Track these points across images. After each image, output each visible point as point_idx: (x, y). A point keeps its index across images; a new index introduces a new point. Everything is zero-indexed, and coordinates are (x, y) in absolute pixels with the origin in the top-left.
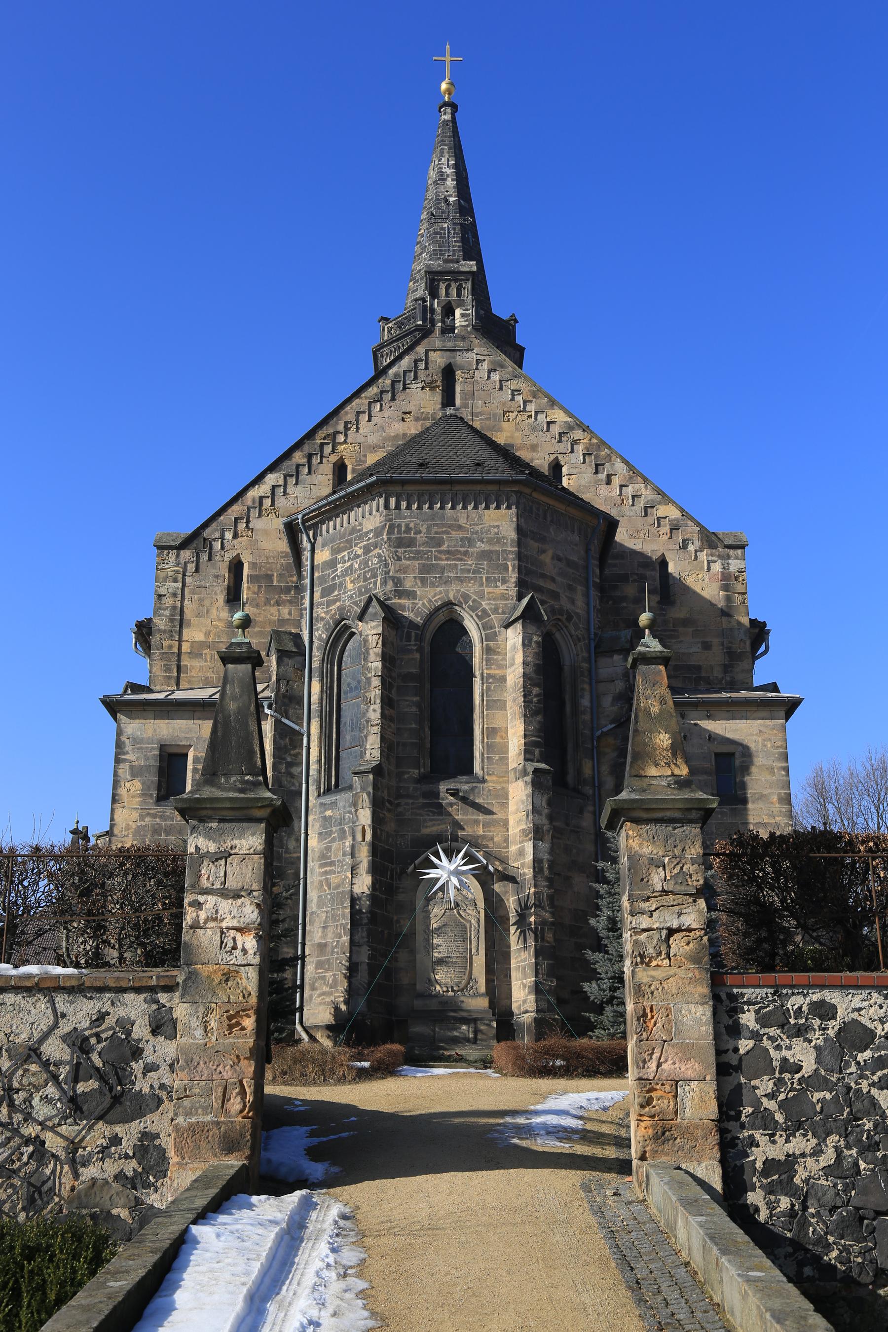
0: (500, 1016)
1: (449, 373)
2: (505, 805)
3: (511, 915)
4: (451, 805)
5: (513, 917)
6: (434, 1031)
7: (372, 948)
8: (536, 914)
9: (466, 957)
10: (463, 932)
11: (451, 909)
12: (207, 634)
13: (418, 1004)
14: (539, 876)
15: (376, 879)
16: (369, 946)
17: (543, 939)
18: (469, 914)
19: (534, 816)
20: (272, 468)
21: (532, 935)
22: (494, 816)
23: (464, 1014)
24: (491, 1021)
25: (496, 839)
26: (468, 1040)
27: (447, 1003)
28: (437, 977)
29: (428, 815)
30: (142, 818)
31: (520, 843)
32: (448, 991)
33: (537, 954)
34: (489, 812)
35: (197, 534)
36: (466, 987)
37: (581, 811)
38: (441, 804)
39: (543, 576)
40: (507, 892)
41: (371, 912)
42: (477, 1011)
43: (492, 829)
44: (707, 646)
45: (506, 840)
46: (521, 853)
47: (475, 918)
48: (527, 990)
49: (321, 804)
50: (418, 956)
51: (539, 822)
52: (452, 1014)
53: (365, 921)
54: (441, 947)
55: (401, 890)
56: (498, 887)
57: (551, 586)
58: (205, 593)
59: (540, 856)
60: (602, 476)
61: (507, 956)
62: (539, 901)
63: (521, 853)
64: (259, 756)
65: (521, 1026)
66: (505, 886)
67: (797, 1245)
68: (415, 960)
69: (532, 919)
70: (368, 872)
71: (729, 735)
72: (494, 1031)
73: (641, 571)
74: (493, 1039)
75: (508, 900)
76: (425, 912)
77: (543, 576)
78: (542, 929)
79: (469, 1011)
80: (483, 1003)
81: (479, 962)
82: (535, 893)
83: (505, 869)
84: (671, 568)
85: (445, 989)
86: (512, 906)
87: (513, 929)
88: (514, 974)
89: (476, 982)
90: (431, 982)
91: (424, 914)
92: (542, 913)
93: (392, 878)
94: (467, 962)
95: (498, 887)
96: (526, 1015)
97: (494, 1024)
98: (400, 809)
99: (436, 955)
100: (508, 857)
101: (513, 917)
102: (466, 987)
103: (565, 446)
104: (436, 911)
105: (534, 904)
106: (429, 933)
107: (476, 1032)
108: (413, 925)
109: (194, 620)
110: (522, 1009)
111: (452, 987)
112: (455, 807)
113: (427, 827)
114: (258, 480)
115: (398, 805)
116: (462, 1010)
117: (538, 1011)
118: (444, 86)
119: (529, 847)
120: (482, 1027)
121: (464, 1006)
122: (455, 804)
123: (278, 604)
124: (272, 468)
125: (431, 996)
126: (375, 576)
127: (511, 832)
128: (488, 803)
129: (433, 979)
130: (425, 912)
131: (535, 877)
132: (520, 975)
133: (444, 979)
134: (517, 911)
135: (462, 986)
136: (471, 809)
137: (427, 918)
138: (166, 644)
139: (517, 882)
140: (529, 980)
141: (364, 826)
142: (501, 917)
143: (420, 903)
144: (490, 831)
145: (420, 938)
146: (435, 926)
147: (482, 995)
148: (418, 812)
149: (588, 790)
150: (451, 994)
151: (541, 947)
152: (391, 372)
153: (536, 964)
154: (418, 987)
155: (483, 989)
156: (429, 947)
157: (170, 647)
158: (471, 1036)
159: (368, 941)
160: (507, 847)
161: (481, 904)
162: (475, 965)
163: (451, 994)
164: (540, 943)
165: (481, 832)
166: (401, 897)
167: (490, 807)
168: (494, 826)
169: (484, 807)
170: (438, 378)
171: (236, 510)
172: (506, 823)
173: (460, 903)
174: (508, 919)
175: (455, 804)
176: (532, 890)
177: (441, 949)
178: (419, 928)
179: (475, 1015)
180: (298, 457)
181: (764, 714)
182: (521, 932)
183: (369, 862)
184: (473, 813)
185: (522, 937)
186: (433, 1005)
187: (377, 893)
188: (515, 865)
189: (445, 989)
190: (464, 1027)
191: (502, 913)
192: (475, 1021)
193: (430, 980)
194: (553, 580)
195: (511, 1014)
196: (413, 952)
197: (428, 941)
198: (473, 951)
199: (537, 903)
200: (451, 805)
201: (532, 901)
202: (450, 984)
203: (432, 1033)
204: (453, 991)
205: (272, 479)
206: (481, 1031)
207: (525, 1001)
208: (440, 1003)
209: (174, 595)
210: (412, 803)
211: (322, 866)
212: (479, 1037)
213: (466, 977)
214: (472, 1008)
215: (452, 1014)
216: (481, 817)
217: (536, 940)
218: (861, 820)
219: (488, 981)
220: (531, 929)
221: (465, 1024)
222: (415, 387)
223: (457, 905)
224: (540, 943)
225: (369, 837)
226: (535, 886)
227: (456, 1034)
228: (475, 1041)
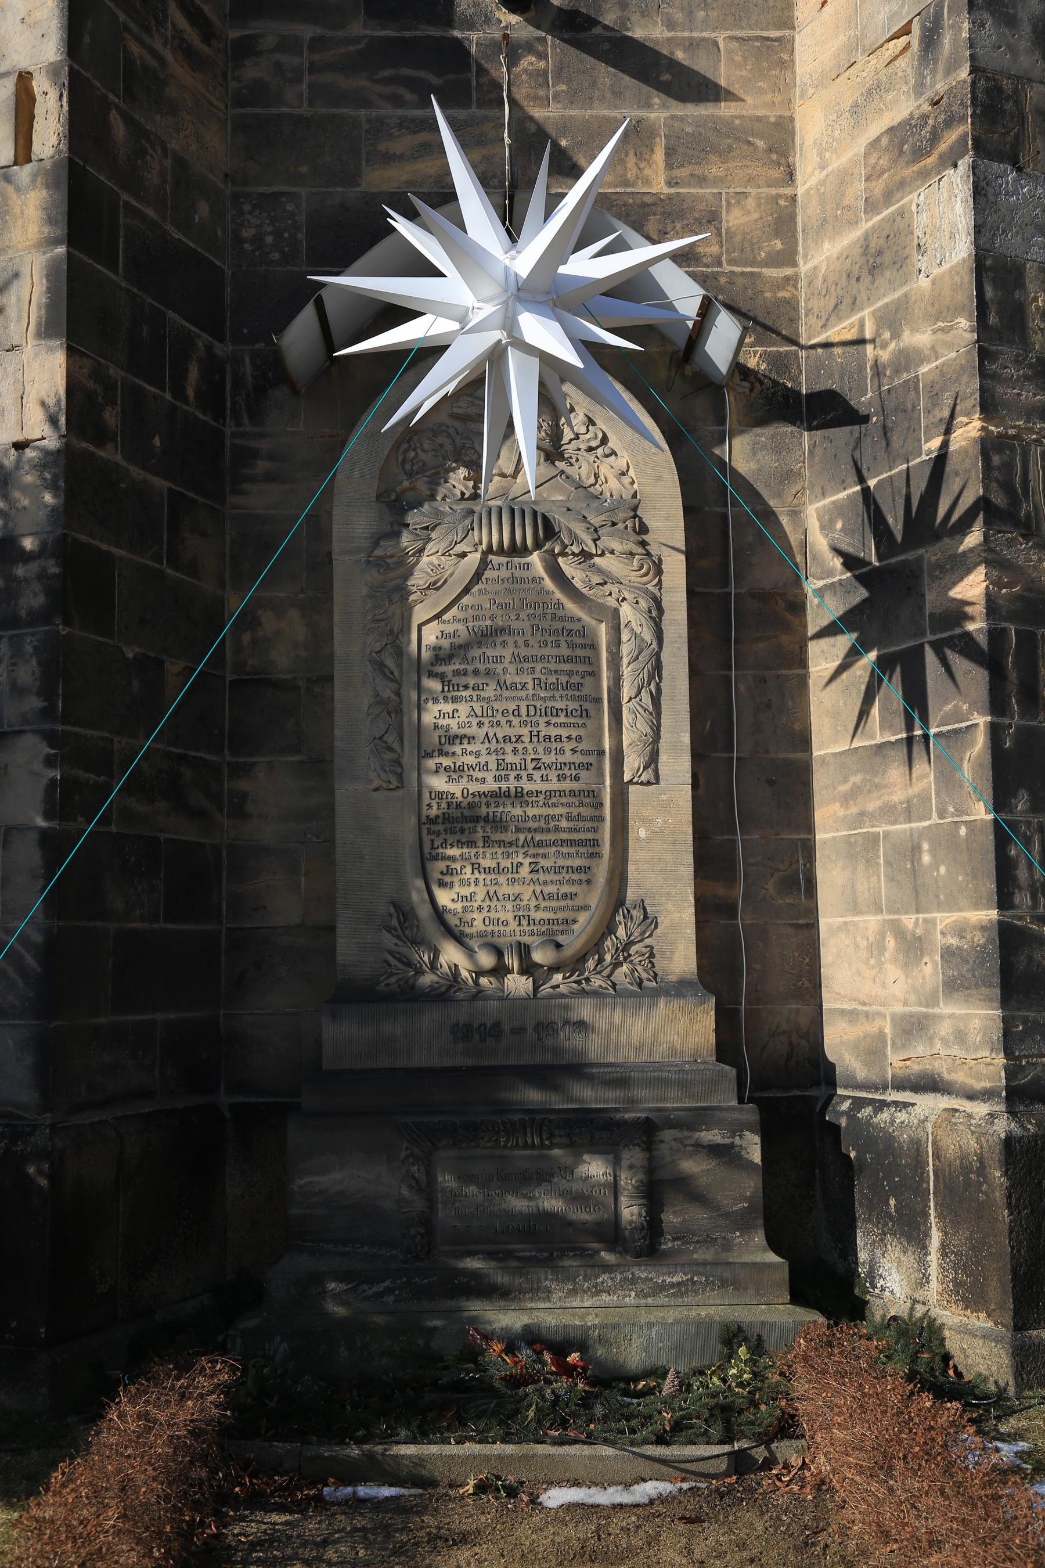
0: (761, 1083)
2: (775, 53)
3: (811, 586)
4: (513, 50)
5: (825, 591)
6: (427, 1189)
7: (65, 750)
9: (593, 796)
10: (574, 663)
11: (517, 550)
13: (344, 1037)
14: (1007, 352)
15: (98, 374)
16: (51, 738)
18: (607, 578)
19: (977, 25)
21: (974, 678)
22: (725, 110)
23: (594, 1097)
24: (736, 1129)
25: (734, 219)
26: (611, 1234)
27: (494, 1030)
28: (444, 898)
29: (397, 101)
31: (871, 206)
32: (500, 971)
33: (1006, 775)
34: (698, 88)
36: (596, 946)
38: (460, 48)
40: (788, 476)
41: (62, 548)
42: (659, 1075)
43: (715, 170)
45: (783, 221)
46: (883, 256)
47: (640, 599)
48: (930, 970)
50: (345, 792)
51: (999, 60)
52: (533, 1096)
53: (33, 599)
54: (473, 739)
55: (262, 466)
56: (745, 453)
59: (1009, 244)
61: (790, 787)
62: (1007, 487)
63: (883, 256)
66: (778, 448)
67: (905, 1107)
68: (330, 809)
69: (973, 587)
70: (46, 331)
72: (751, 1186)
74: (742, 1222)
75: (795, 514)
76: (381, 564)
78: (1027, 641)
79: (618, 1078)
80: (686, 1030)
81: (662, 821)
82: (987, 446)
83: (780, 362)
85: (487, 960)
86: (820, 542)
87: (823, 657)
88: (831, 879)
89: (650, 922)
90: (414, 925)
91: (373, 576)
92: (1022, 552)
93: (212, 397)
94: (598, 829)
95: (745, 453)
96: (928, 1106)
97: (753, 1149)
98: (252, 71)
99: (438, 783)
100: (791, 304)
101: (825, 591)
102: (596, 946)
104: (442, 567)
105: (983, 505)
106: (401, 674)
107: (654, 1192)
108: (321, 638)
110: (895, 1062)
111: (523, 951)
112: (528, 61)
113: (389, 159)
115: (245, 49)
116: (577, 1070)
117: (1018, 1095)
120: (691, 1166)
121: (588, 1047)
122: (529, 47)
125: (410, 996)
128: (692, 45)
129: (424, 912)
130: (381, 564)
131: (984, 354)
132: (876, 882)
133: (485, 907)
134: (850, 562)
135: (573, 942)
136: (606, 74)
137: (393, 591)
139: (853, 417)
140: (944, 919)
141: (24, 79)
142: (765, 597)
144: (702, 180)
145: (352, 699)
146: (431, 636)
147: (678, 989)
148: (346, 83)
150: (518, 984)
151: (1025, 736)
153: (1001, 838)
154: (348, 948)
155: (681, 957)
156: (404, 747)
158: (630, 1211)
159: (47, 713)
160: (788, 257)
161: (668, 525)
162: (638, 832)
163: (518, 984)
164: (1015, 720)
165: (659, 186)
166: (259, 499)
167: (701, 64)
168: (724, 154)
169: (673, 65)
172: (779, 142)
173: (560, 519)
174: (798, 607)
175: (529, 47)
176: (969, 429)
177: (464, 756)
178: (350, 647)
179: (651, 1101)
182: (884, 664)
183: (52, 273)
184: (618, 94)
185: (893, 691)
186: (426, 1042)
187: (111, 454)
188: (840, 331)
189: (487, 960)
190: (595, 1169)
191: (764, 577)
192: (646, 1131)
193: (404, 914)
195: (822, 1073)
196: (320, 768)
198: (632, 763)
199: (999, 499)
200: (513, 50)
201: (965, 487)
202: (513, 931)
203: (419, 1204)
204: (528, 968)
208: (463, 1032)
210: (317, 43)
212: (670, 1218)
213: (595, 897)
214: (628, 1056)
215: (533, 1096)
216: (661, 112)
217: (997, 705)
219: (708, 910)
220: (967, 646)
221: (596, 1147)
223: (548, 530)
224: (1015, 720)
225: (49, 134)
226: (988, 407)
227: (551, 1203)
228: (648, 1244)
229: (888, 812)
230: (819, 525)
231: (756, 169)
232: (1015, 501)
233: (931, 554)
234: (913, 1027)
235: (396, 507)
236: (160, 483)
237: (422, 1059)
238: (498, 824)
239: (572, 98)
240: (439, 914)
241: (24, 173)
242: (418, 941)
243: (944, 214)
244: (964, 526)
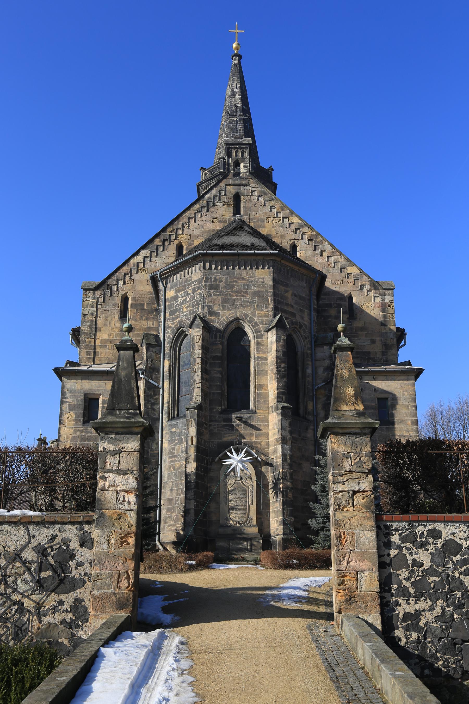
0: (264, 537)
1: (237, 197)
2: (267, 426)
3: (270, 484)
4: (238, 425)
5: (271, 485)
6: (229, 545)
7: (196, 501)
8: (283, 483)
9: (246, 506)
10: (244, 492)
11: (238, 480)
12: (109, 335)
13: (221, 530)
14: (285, 463)
15: (199, 465)
16: (195, 500)
18: (248, 483)
19: (282, 431)
20: (144, 247)
21: (281, 494)
22: (261, 432)
23: (245, 536)
24: (260, 540)
25: (262, 444)
26: (247, 550)
27: (236, 530)
28: (231, 516)
29: (226, 431)
30: (75, 432)
31: (275, 445)
32: (236, 524)
33: (284, 504)
34: (258, 429)
35: (104, 282)
36: (246, 521)
37: (307, 429)
38: (233, 425)
39: (287, 304)
40: (268, 471)
41: (196, 482)
42: (252, 534)
43: (260, 438)
44: (373, 342)
45: (267, 444)
46: (275, 451)
47: (251, 485)
48: (278, 523)
49: (170, 425)
50: (221, 505)
52: (239, 536)
53: (193, 487)
54: (233, 500)
55: (212, 470)
56: (263, 469)
57: (291, 310)
58: (108, 313)
59: (285, 452)
60: (318, 252)
61: (268, 505)
62: (285, 476)
63: (275, 451)
64: (137, 399)
66: (267, 468)
67: (421, 658)
68: (219, 507)
69: (281, 486)
70: (194, 461)
71: (385, 389)
72: (261, 545)
73: (339, 302)
75: (268, 476)
76: (225, 482)
77: (287, 304)
78: (286, 491)
79: (247, 534)
80: (255, 530)
81: (253, 508)
82: (283, 472)
83: (267, 459)
84: (354, 300)
85: (235, 523)
86: (271, 479)
87: (271, 491)
88: (271, 515)
89: (252, 519)
90: (228, 519)
92: (286, 482)
93: (207, 464)
94: (247, 509)
95: (263, 469)
96: (278, 537)
97: (261, 541)
98: (211, 428)
99: (230, 505)
100: (268, 453)
101: (271, 485)
102: (246, 521)
103: (298, 236)
104: (230, 481)
106: (226, 493)
107: (251, 545)
108: (218, 489)
109: (103, 328)
111: (239, 522)
113: (225, 437)
114: (136, 253)
115: (210, 425)
116: (244, 534)
117: (284, 534)
118: (234, 45)
120: (255, 543)
121: (245, 531)
122: (240, 425)
123: (147, 319)
124: (144, 247)
125: (227, 526)
126: (198, 304)
128: (258, 425)
129: (229, 518)
130: (225, 482)
131: (282, 463)
132: (274, 515)
133: (235, 517)
134: (273, 482)
135: (244, 521)
136: (248, 428)
137: (226, 485)
138: (87, 340)
140: (279, 518)
141: (192, 437)
142: (265, 485)
143: (222, 477)
144: (259, 439)
145: (222, 496)
146: (230, 489)
148: (221, 429)
149: (310, 417)
150: (238, 525)
152: (207, 197)
154: (221, 521)
155: (255, 523)
156: (227, 500)
157: (90, 342)
159: (194, 498)
160: (268, 448)
161: (254, 478)
162: (251, 510)
163: (238, 525)
165: (254, 440)
166: (212, 474)
168: (261, 437)
169: (256, 427)
170: (231, 200)
171: (125, 269)
172: (267, 435)
173: (243, 477)
174: (268, 486)
175: (240, 425)
176: (281, 470)
178: (221, 490)
179: (251, 537)
180: (158, 242)
181: (403, 377)
182: (275, 493)
183: (195, 456)
184: (250, 430)
185: (276, 495)
186: (229, 531)
187: (199, 472)
188: (272, 457)
189: (235, 523)
190: (245, 543)
191: (265, 483)
192: (251, 539)
193: (227, 518)
194: (292, 306)
195: (270, 536)
196: (218, 503)
197: (226, 497)
198: (250, 503)
199: (284, 477)
200: (238, 425)
201: (281, 476)
202: (238, 520)
204: (239, 524)
205: (144, 253)
206: (254, 545)
208: (233, 530)
209: (92, 314)
210: (218, 425)
211: (170, 458)
212: (253, 548)
213: (246, 516)
214: (249, 533)
215: (239, 536)
216: (254, 432)
218: (455, 433)
219: (258, 519)
220: (280, 491)
221: (245, 541)
222: (219, 205)
225: (195, 442)
226: (283, 468)
227: (241, 546)
228: (251, 550)
229: (276, 508)
230: (270, 477)
231: (265, 438)
232: (285, 477)
233: (279, 482)
234: (277, 529)
235: (226, 476)
236: (203, 474)
237: (229, 533)
238: (236, 509)
239: (245, 430)
240: (230, 518)
241: (192, 446)
242: (228, 521)
243: (279, 447)
244: (280, 480)
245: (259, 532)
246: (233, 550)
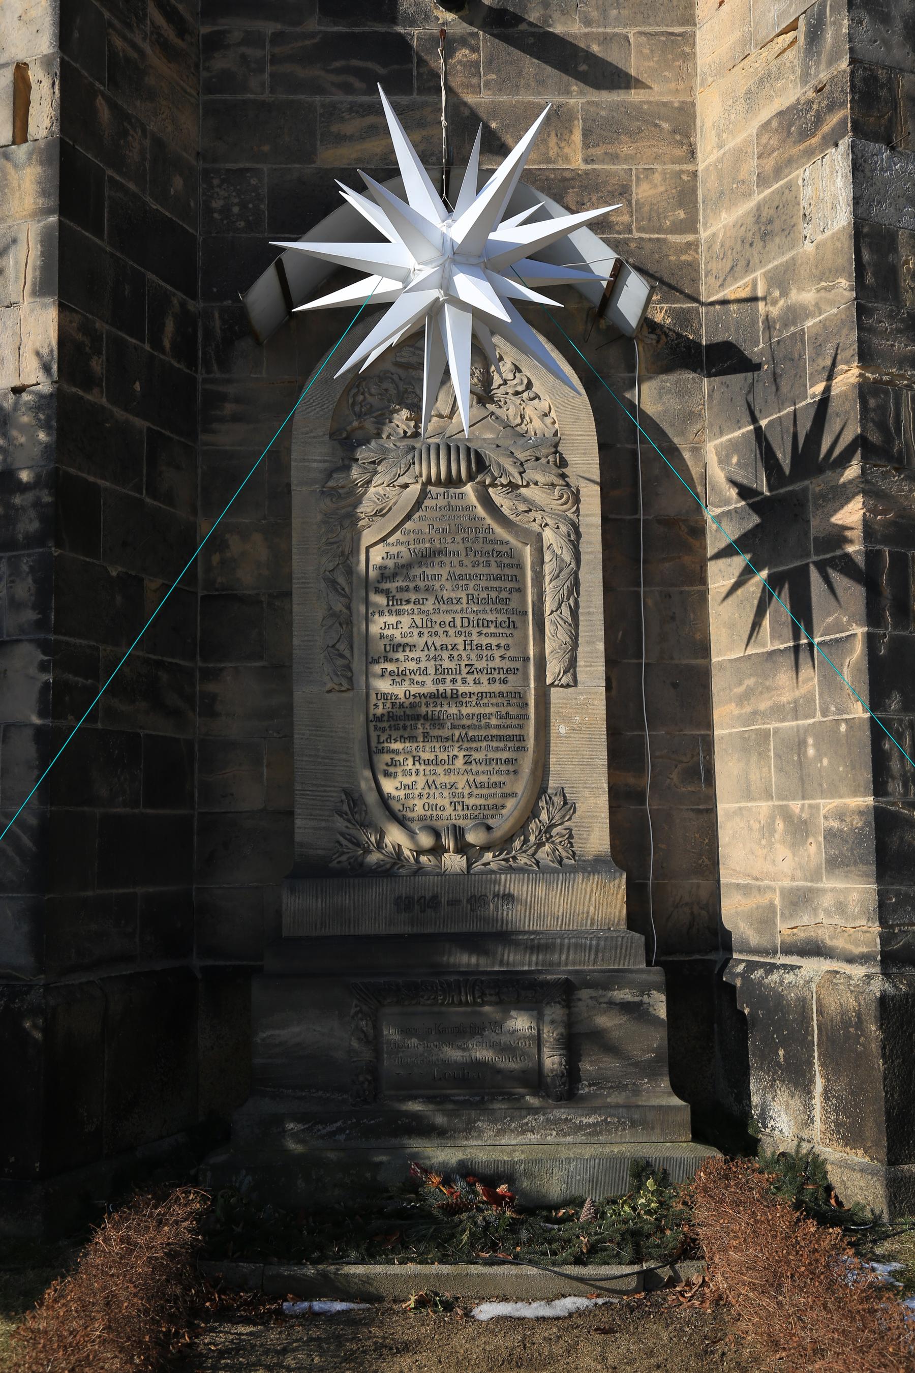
0: (667, 948)
2: (678, 46)
3: (710, 513)
4: (449, 44)
5: (723, 518)
6: (374, 1041)
7: (57, 657)
8: (866, 487)
9: (519, 697)
10: (503, 581)
11: (453, 482)
13: (302, 908)
14: (882, 308)
15: (86, 328)
16: (44, 646)
17: (902, 610)
18: (531, 506)
19: (856, 22)
21: (853, 593)
22: (635, 96)
23: (520, 961)
24: (645, 989)
25: (643, 192)
26: (535, 1080)
27: (433, 902)
28: (389, 786)
29: (348, 89)
31: (763, 181)
32: (437, 850)
33: (881, 678)
34: (611, 77)
36: (522, 828)
38: (402, 42)
40: (690, 416)
41: (55, 480)
42: (577, 941)
43: (626, 149)
45: (686, 194)
46: (773, 225)
47: (560, 524)
48: (814, 850)
50: (302, 693)
51: (875, 52)
52: (466, 960)
53: (29, 524)
54: (414, 647)
55: (229, 408)
56: (652, 397)
59: (884, 213)
61: (692, 689)
62: (882, 426)
63: (773, 225)
65: (788, 1018)
66: (682, 392)
68: (289, 708)
69: (852, 514)
70: (40, 290)
72: (658, 1038)
75: (696, 450)
76: (333, 494)
78: (899, 561)
79: (541, 944)
80: (600, 902)
81: (580, 718)
82: (865, 390)
83: (683, 317)
85: (426, 841)
87: (721, 576)
88: (728, 770)
89: (569, 807)
90: (362, 810)
91: (327, 504)
92: (894, 483)
93: (185, 347)
94: (524, 726)
95: (652, 397)
96: (812, 968)
97: (660, 1006)
98: (221, 62)
99: (384, 686)
100: (693, 267)
101: (723, 518)
102: (522, 828)
104: (387, 496)
105: (860, 442)
106: (351, 590)
107: (573, 1044)
108: (281, 559)
110: (784, 930)
111: (458, 833)
112: (462, 54)
113: (340, 139)
115: (214, 43)
116: (505, 936)
117: (891, 959)
119: (827, 187)
120: (605, 1021)
121: (515, 916)
122: (463, 41)
125: (359, 872)
127: (708, 155)
128: (606, 40)
129: (372, 798)
130: (333, 494)
131: (861, 310)
132: (768, 772)
133: (424, 794)
134: (745, 492)
135: (502, 825)
136: (530, 65)
137: (344, 518)
139: (747, 365)
140: (827, 805)
141: (21, 69)
142: (669, 523)
143: (309, 456)
144: (614, 158)
145: (308, 612)
146: (377, 557)
147: (593, 866)
148: (303, 73)
150: (453, 862)
151: (898, 644)
153: (877, 734)
154: (306, 830)
155: (597, 838)
156: (353, 654)
158: (552, 1061)
159: (41, 624)
160: (690, 225)
161: (585, 460)
162: (559, 729)
163: (453, 862)
164: (889, 631)
165: (577, 162)
166: (227, 437)
167: (613, 56)
168: (634, 135)
169: (590, 57)
172: (682, 124)
173: (490, 454)
174: (699, 531)
175: (463, 41)
176: (849, 376)
177: (407, 662)
178: (307, 566)
179: (569, 964)
182: (774, 581)
183: (45, 239)
184: (541, 83)
185: (782, 605)
186: (373, 913)
187: (97, 398)
188: (736, 290)
189: (426, 841)
190: (521, 1023)
191: (669, 506)
192: (566, 991)
193: (354, 800)
195: (720, 940)
196: (280, 673)
197: (346, 624)
198: (554, 668)
199: (875, 437)
200: (449, 44)
201: (845, 427)
202: (450, 815)
204: (462, 848)
206: (599, 1039)
207: (799, 900)
208: (405, 904)
210: (277, 38)
212: (587, 1066)
213: (521, 786)
214: (550, 925)
215: (466, 960)
216: (579, 98)
217: (873, 617)
219: (620, 797)
220: (847, 565)
221: (522, 1005)
224: (889, 631)
225: (43, 118)
226: (865, 356)
227: (483, 1054)
228: (567, 1089)
229: (778, 711)
230: (717, 460)
231: (662, 148)
232: (888, 439)
233: (815, 485)
235: (347, 444)
236: (140, 423)
237: (369, 927)
238: (436, 721)
239: (501, 86)
240: (384, 800)
241: (21, 152)
242: (366, 824)
244: (844, 460)
245: (636, 919)
246: (409, 1087)
